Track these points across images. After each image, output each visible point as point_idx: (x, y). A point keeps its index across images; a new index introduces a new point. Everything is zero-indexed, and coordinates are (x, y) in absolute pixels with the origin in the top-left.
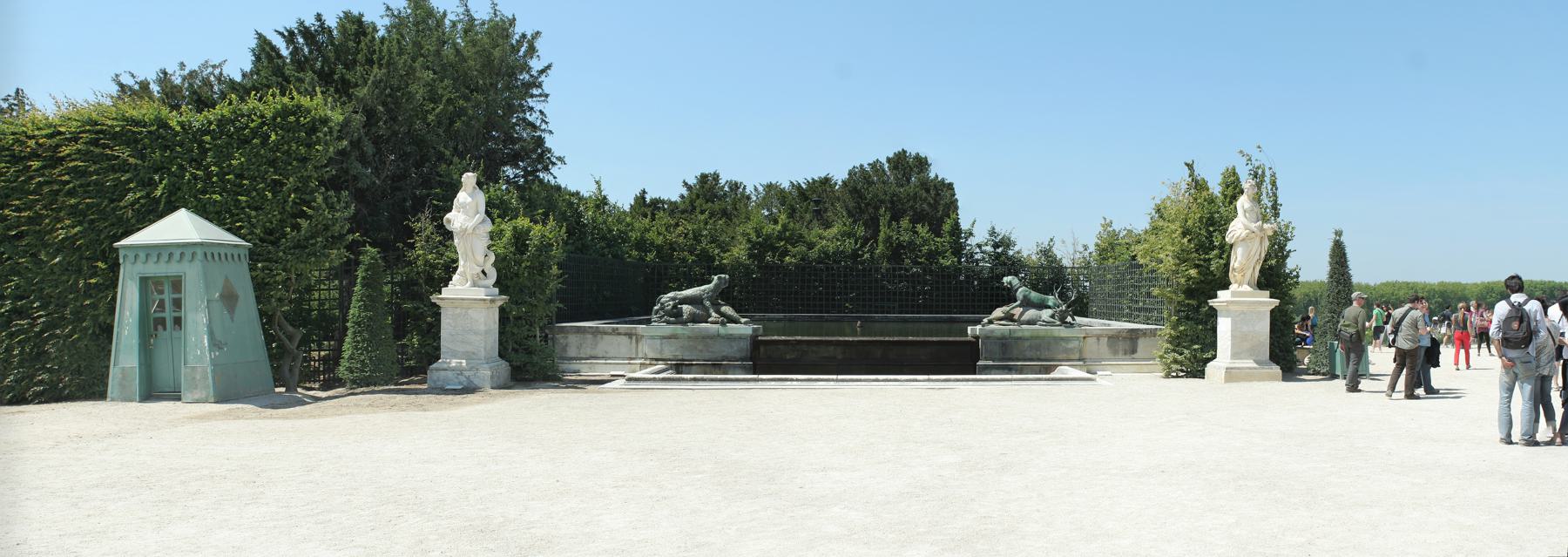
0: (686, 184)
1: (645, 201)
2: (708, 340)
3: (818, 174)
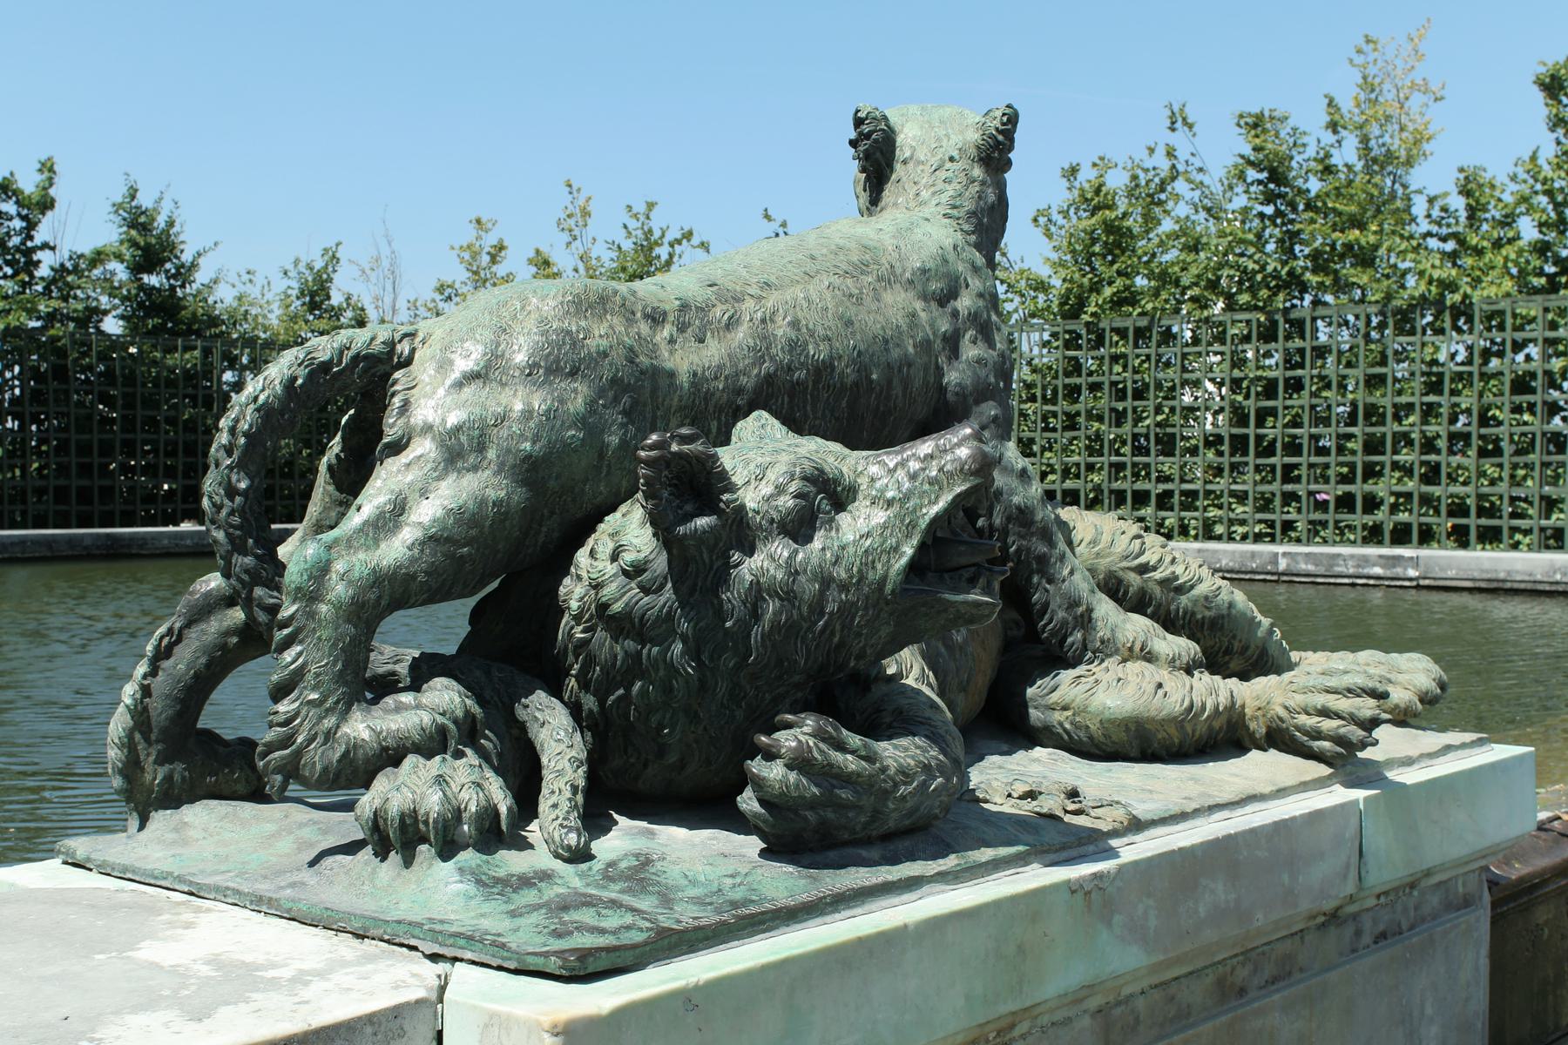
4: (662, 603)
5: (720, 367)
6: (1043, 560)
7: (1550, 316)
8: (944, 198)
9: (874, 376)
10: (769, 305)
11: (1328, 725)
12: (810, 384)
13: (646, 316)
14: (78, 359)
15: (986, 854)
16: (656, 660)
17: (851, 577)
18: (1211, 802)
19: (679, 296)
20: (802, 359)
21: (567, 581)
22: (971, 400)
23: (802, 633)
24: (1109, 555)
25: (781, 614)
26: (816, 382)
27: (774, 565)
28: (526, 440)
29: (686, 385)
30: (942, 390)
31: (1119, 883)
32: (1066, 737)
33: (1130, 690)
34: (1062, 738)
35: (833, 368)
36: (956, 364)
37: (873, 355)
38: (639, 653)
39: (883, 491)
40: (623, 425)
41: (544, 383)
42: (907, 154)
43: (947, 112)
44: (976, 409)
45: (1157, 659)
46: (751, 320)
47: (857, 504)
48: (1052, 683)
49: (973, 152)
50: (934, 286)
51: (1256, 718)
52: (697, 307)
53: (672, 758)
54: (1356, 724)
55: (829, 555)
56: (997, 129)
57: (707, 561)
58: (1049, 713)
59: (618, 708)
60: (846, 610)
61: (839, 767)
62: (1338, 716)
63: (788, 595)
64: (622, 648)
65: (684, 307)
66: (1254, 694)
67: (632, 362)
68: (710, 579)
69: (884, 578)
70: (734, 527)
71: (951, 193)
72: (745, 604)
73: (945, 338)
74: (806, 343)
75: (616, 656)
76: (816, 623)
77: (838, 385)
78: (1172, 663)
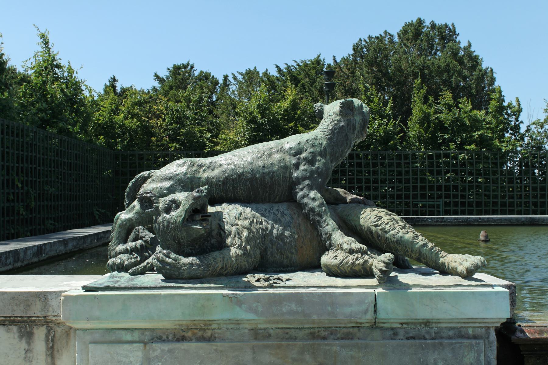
0: (157, 77)
1: (115, 91)
2: (335, 346)
3: (310, 56)
6: (319, 222)
14: (532, 160)
15: (213, 285)
24: (368, 221)
31: (243, 297)
73: (294, 165)
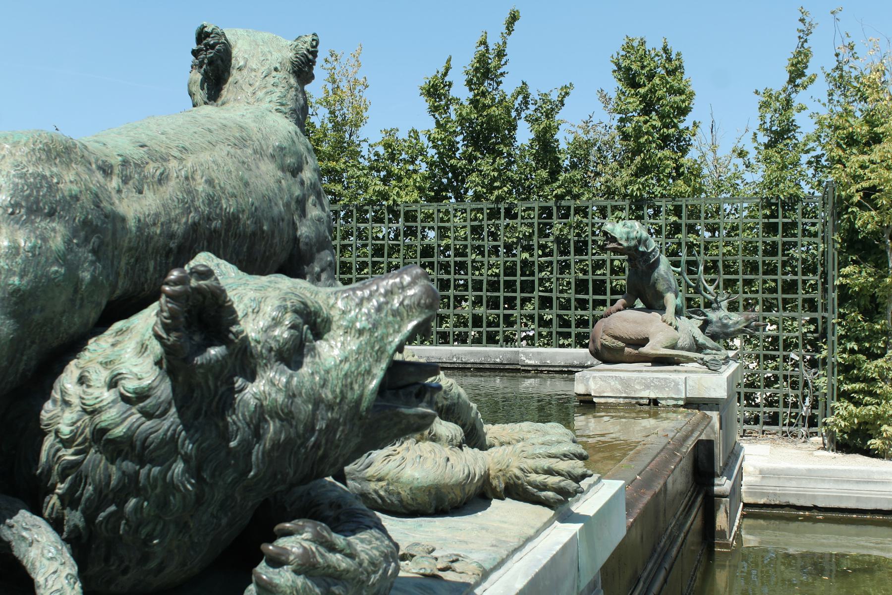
4: (166, 427)
5: (157, 215)
7: (441, 215)
8: (275, 97)
9: (265, 228)
10: (189, 165)
11: (552, 480)
12: (223, 232)
13: (100, 168)
16: (156, 479)
17: (335, 398)
18: (511, 549)
19: (120, 153)
20: (218, 211)
21: (48, 405)
22: (314, 249)
23: (295, 449)
25: (281, 432)
26: (227, 231)
27: (274, 389)
28: (14, 274)
29: (134, 229)
30: (296, 240)
32: (380, 501)
33: (429, 464)
34: (376, 502)
35: (238, 219)
36: (304, 221)
37: (264, 210)
38: (137, 473)
39: (353, 322)
40: (93, 263)
41: (26, 222)
42: (242, 63)
43: (267, 35)
44: (318, 256)
45: (440, 440)
46: (178, 177)
47: (331, 333)
48: (367, 461)
49: (289, 66)
50: (289, 160)
51: (498, 477)
52: (135, 164)
53: (153, 564)
54: (572, 479)
55: (317, 378)
56: (308, 50)
57: (212, 387)
58: (365, 484)
59: (107, 522)
60: (332, 426)
61: (335, 567)
62: (559, 473)
63: (286, 416)
64: (119, 469)
65: (125, 163)
66: (496, 460)
67: (98, 207)
68: (214, 404)
69: (361, 396)
70: (239, 356)
71: (279, 94)
72: (248, 425)
74: (220, 198)
75: (110, 476)
76: (308, 439)
77: (242, 234)
78: (450, 442)
